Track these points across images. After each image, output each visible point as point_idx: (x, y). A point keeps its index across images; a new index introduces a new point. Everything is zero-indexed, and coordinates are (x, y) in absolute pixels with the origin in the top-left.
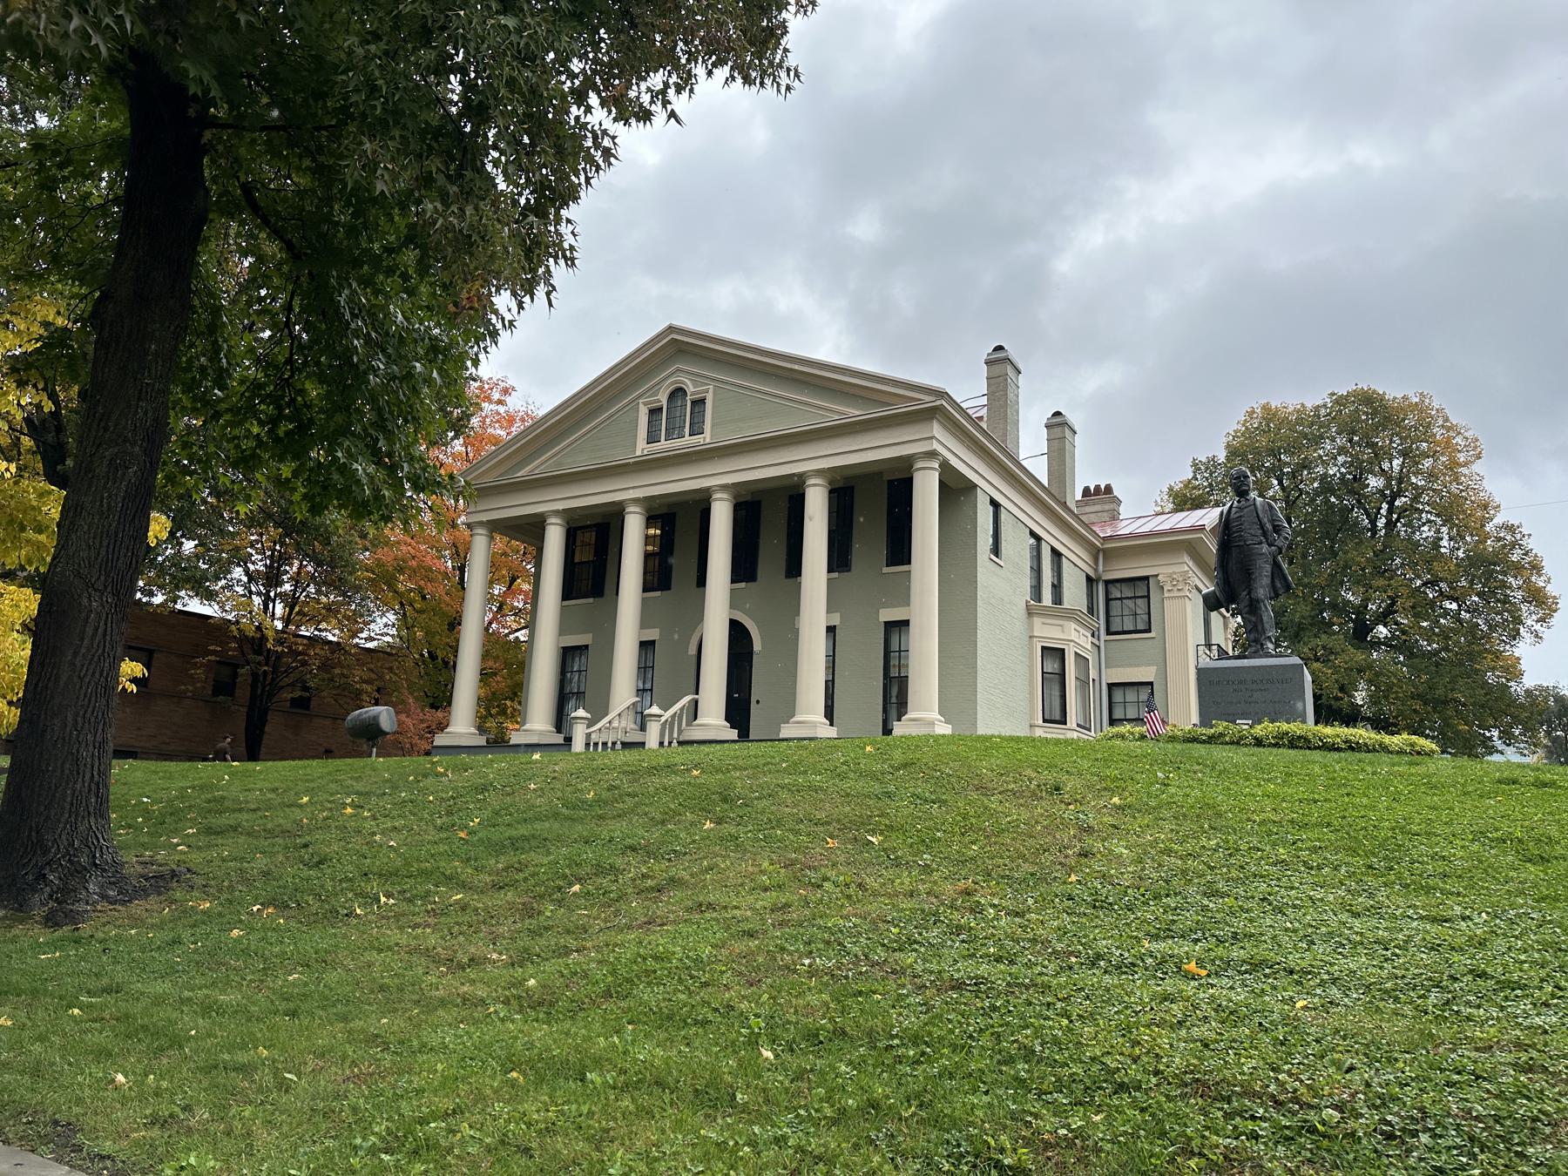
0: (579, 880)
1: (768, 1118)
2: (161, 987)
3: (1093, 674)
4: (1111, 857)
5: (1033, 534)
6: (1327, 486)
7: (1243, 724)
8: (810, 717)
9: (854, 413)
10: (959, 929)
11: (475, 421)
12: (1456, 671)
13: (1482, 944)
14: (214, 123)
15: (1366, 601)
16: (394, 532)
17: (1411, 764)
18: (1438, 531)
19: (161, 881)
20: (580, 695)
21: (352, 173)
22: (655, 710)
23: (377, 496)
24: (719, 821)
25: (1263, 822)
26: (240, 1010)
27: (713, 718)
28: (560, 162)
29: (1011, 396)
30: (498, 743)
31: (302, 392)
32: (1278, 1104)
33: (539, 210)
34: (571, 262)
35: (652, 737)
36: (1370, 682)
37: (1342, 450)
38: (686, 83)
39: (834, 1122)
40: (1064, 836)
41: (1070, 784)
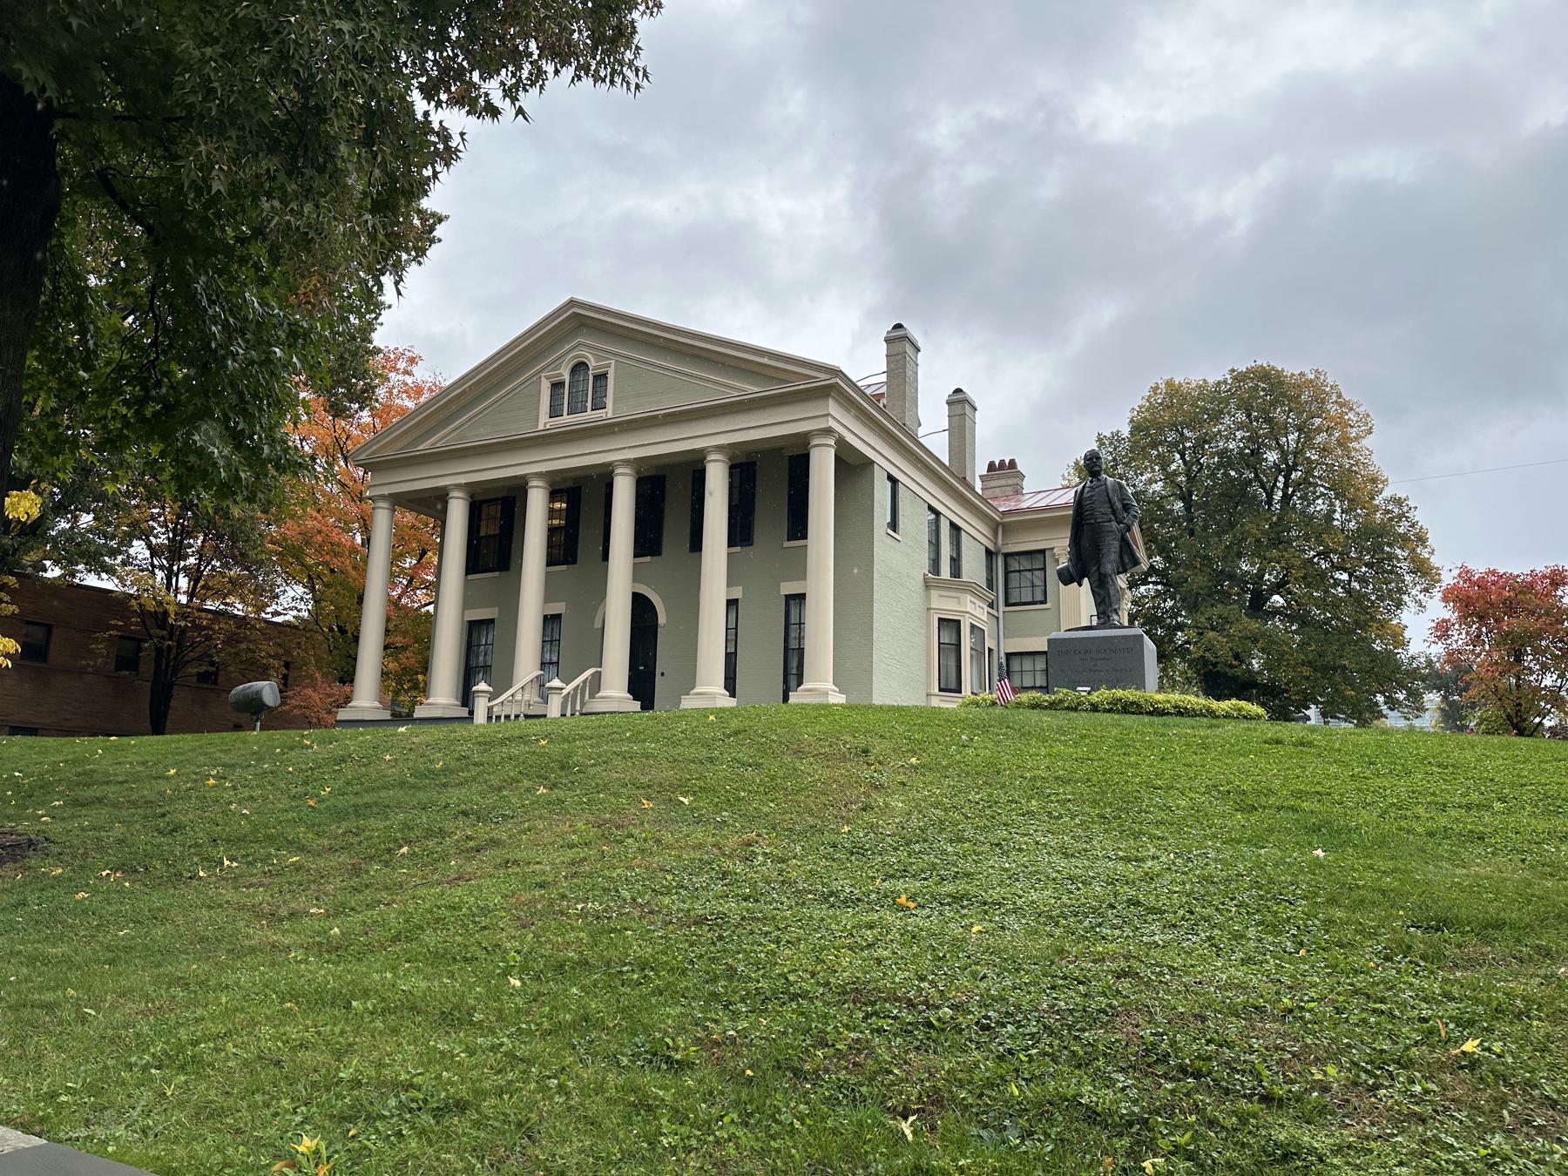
0: (409, 843)
5: (931, 508)
8: (710, 688)
9: (753, 389)
11: (381, 392)
12: (1344, 639)
17: (1210, 727)
18: (1332, 504)
22: (556, 683)
25: (1034, 778)
26: (67, 960)
27: (615, 690)
29: (909, 373)
35: (554, 708)
36: (1263, 650)
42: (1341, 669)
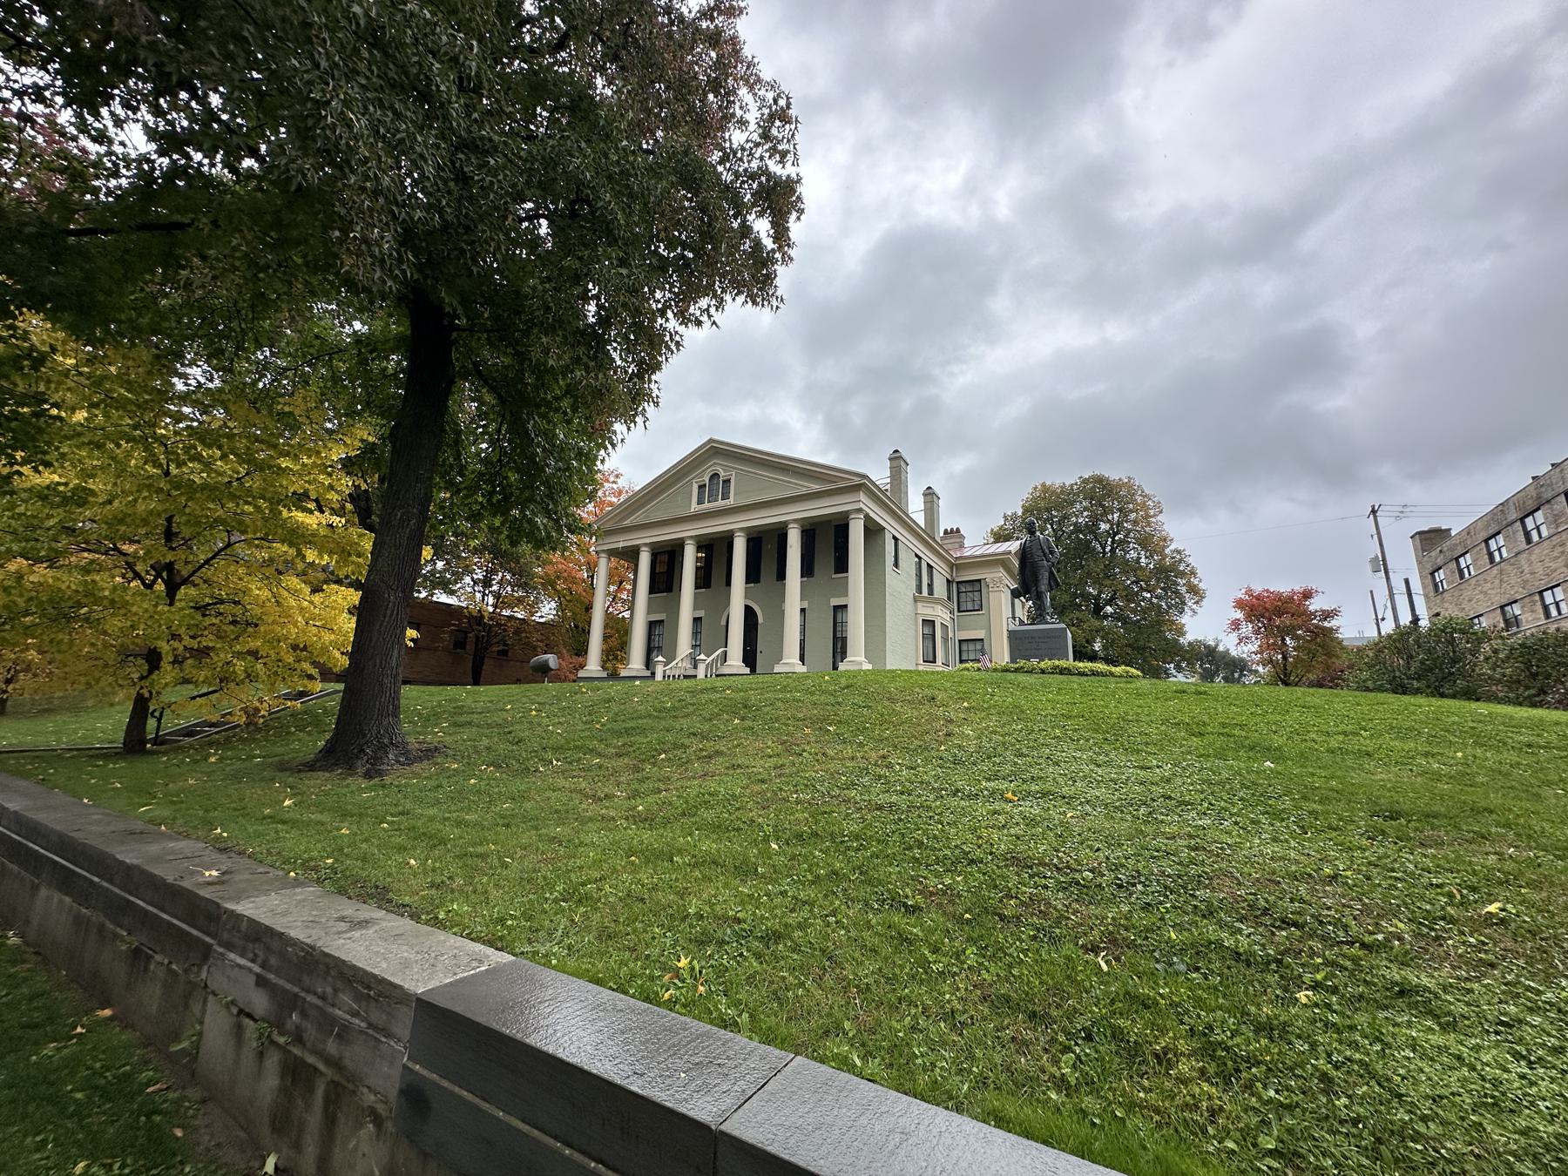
1: (776, 881)
2: (431, 812)
3: (951, 635)
4: (963, 736)
6: (1078, 528)
7: (1034, 661)
8: (791, 661)
9: (815, 487)
10: (880, 777)
11: (600, 493)
13: (1168, 781)
14: (459, 328)
15: (1100, 592)
16: (556, 557)
19: (429, 753)
20: (660, 648)
21: (536, 354)
23: (549, 537)
24: (743, 719)
27: (735, 662)
28: (651, 347)
30: (614, 676)
31: (506, 478)
32: (1058, 869)
33: (639, 375)
34: (657, 404)
35: (701, 672)
37: (1086, 509)
38: (720, 305)
39: (813, 882)
40: (937, 725)
41: (940, 696)
42: (1150, 646)
